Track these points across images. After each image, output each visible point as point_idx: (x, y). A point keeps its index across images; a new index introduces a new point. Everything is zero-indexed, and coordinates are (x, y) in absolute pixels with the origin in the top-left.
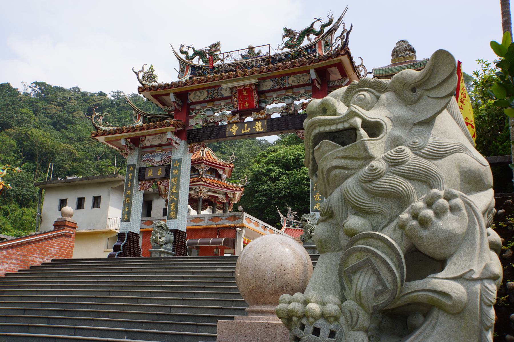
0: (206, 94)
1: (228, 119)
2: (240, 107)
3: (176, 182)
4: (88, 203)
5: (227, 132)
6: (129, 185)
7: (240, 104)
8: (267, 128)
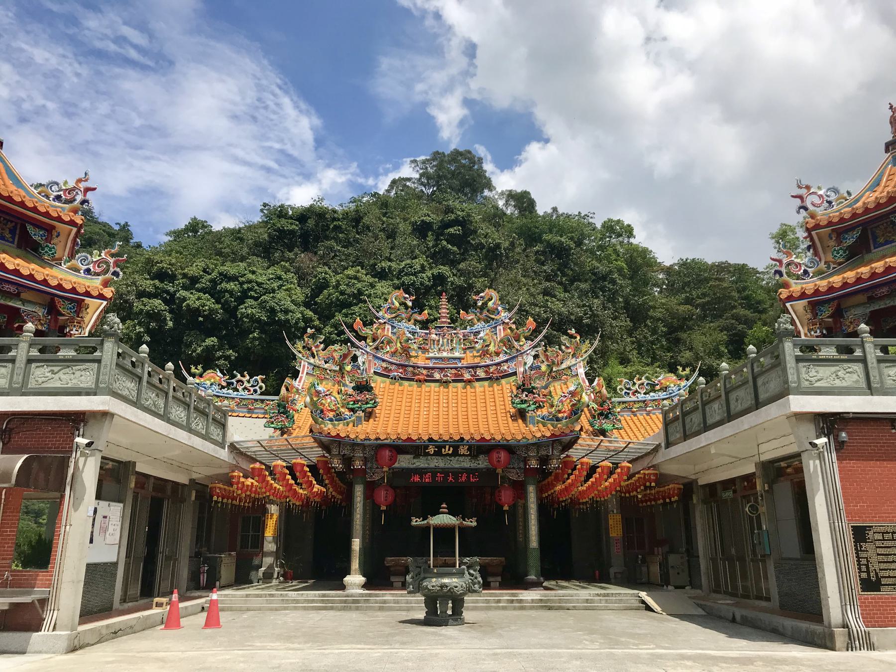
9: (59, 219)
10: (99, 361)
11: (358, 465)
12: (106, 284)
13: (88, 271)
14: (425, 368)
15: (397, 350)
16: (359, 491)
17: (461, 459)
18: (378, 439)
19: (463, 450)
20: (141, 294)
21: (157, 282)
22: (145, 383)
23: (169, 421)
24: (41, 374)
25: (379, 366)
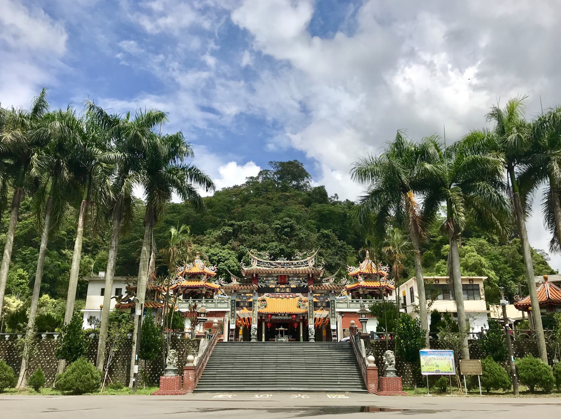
11: (263, 318)
16: (264, 324)
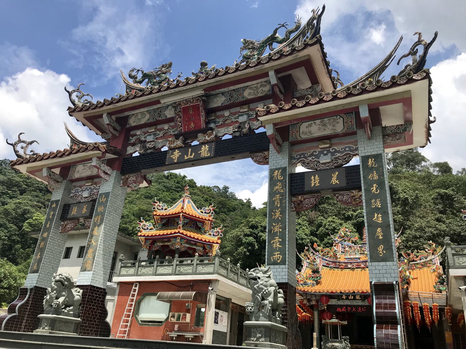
0: (148, 116)
1: (169, 144)
2: (185, 129)
3: (99, 221)
4: (75, 252)
5: (167, 159)
6: (48, 226)
7: (185, 126)
8: (215, 152)
9: (205, 219)
10: (214, 264)
12: (219, 239)
13: (213, 235)
14: (344, 263)
15: (331, 256)
17: (357, 301)
18: (320, 292)
19: (358, 297)
20: (246, 235)
21: (251, 230)
22: (229, 271)
23: (239, 283)
24: (200, 268)
25: (324, 263)
